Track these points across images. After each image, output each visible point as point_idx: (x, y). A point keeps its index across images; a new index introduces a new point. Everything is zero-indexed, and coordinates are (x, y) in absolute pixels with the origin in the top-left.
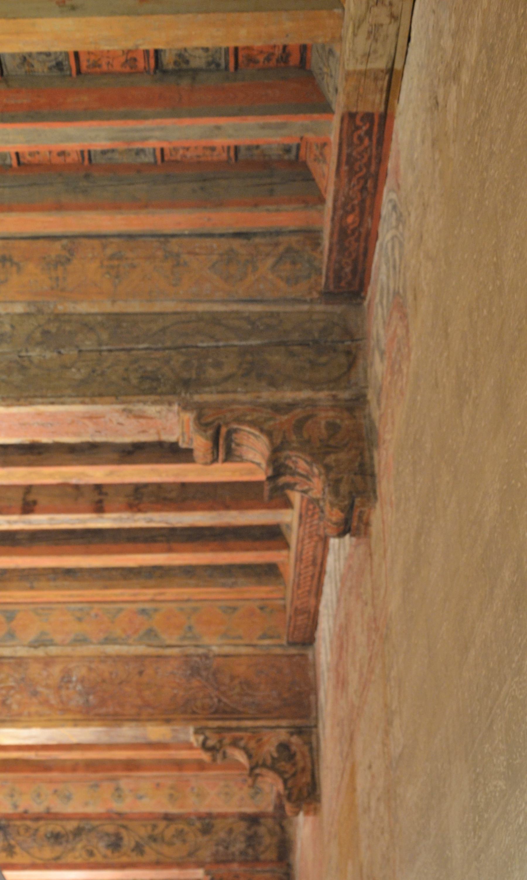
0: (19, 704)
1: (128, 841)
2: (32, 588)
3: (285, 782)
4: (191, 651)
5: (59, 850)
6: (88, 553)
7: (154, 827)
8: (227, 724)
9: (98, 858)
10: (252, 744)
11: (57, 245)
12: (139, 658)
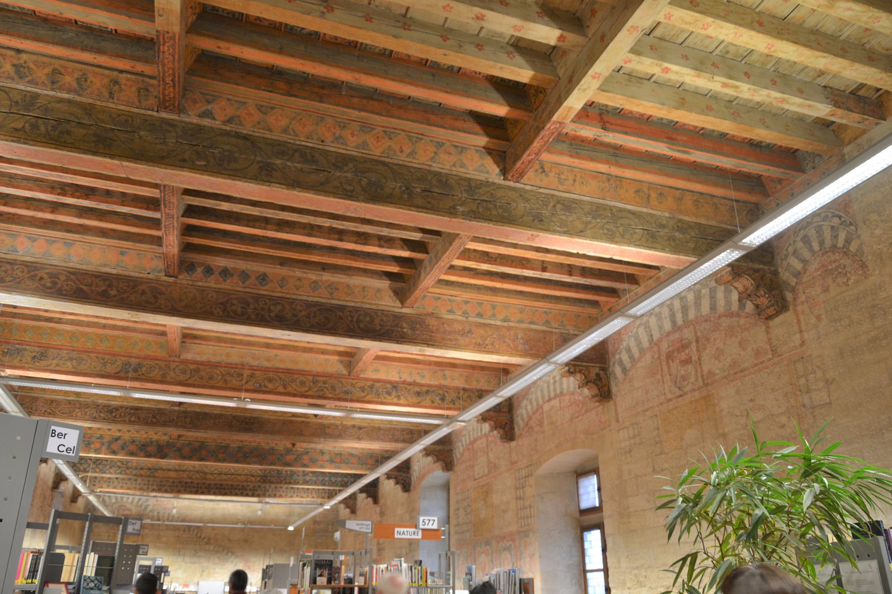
1: (448, 398)
4: (563, 331)
5: (419, 399)
6: (547, 288)
9: (436, 404)
11: (678, 192)
12: (544, 332)
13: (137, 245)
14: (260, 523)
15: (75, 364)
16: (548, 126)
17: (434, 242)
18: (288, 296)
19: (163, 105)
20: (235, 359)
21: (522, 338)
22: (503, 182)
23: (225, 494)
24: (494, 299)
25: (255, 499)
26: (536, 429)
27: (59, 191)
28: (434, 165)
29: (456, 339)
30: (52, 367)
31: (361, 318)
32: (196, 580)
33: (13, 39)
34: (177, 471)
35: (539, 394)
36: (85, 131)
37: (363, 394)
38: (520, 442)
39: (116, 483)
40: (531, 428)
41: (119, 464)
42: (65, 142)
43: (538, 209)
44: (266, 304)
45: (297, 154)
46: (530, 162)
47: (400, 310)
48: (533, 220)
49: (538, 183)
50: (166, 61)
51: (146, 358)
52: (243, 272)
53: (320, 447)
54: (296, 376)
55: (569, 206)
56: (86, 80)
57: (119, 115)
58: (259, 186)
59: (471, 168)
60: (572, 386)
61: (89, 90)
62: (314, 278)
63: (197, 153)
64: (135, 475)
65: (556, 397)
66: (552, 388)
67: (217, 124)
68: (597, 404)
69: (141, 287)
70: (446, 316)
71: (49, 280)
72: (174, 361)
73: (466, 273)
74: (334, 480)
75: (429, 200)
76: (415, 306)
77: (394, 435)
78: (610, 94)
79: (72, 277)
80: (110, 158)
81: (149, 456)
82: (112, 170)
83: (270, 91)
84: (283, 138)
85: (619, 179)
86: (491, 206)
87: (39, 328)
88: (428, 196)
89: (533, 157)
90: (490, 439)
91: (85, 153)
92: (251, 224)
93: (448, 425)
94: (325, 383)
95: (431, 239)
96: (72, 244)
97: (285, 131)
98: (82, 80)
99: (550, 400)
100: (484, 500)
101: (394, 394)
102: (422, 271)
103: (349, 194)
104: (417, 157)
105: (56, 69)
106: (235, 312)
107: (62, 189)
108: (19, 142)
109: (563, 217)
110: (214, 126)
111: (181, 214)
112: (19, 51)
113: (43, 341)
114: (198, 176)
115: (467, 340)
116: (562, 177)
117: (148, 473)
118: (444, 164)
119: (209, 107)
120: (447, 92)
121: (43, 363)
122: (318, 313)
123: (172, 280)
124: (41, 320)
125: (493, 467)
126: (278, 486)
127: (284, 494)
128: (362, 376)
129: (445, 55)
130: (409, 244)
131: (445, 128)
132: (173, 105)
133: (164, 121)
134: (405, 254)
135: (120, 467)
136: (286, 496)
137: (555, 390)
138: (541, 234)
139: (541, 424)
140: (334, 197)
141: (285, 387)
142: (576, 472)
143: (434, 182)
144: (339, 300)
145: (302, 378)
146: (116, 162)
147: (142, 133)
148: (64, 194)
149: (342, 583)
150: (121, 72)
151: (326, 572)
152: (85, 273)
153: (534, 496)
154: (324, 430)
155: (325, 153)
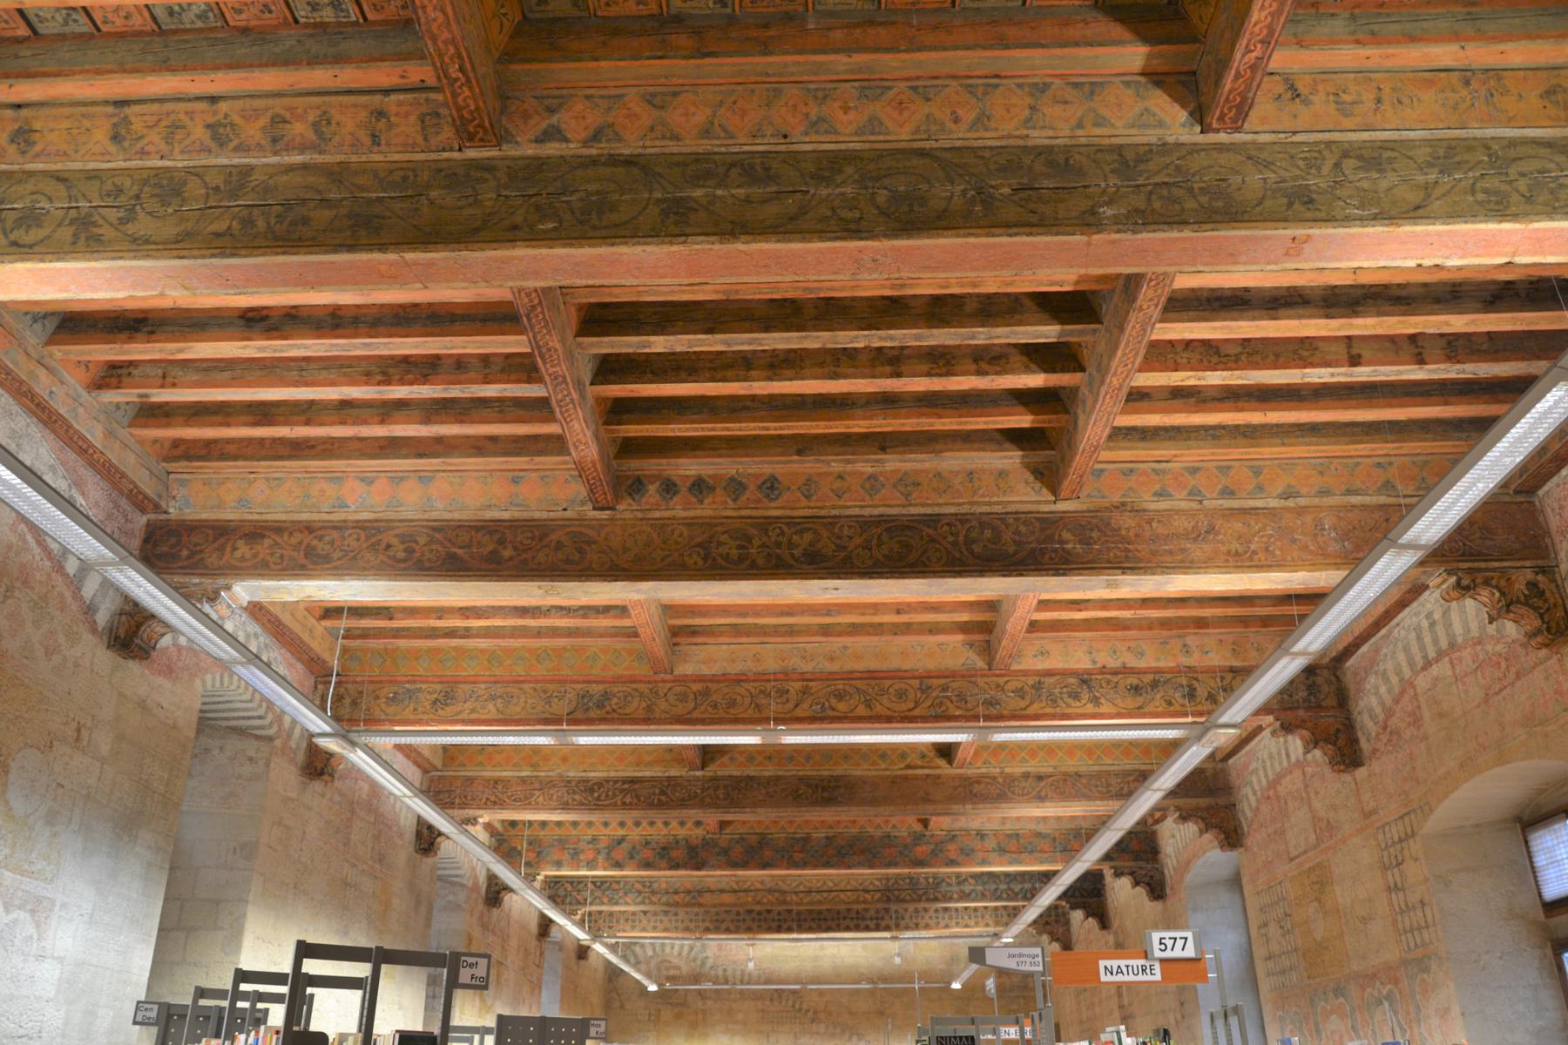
1: (1202, 692)
2: (1284, 444)
3: (1541, 616)
5: (1140, 700)
7: (1222, 678)
8: (1476, 565)
9: (1177, 707)
10: (1503, 583)
13: (537, 459)
14: (901, 979)
17: (1089, 338)
18: (823, 513)
20: (771, 665)
22: (1202, 139)
26: (1407, 734)
27: (379, 377)
28: (1035, 133)
29: (1183, 550)
30: (465, 716)
31: (973, 535)
33: (198, 76)
35: (1401, 657)
36: (334, 212)
37: (1023, 704)
38: (1376, 766)
40: (1396, 733)
41: (638, 886)
42: (300, 239)
43: (1296, 178)
44: (783, 533)
45: (734, 172)
47: (1053, 508)
48: (1290, 205)
49: (1288, 124)
51: (616, 680)
52: (732, 479)
53: (962, 823)
54: (887, 683)
55: (1374, 158)
56: (329, 123)
57: (391, 172)
58: (666, 249)
59: (1119, 124)
60: (1474, 625)
61: (337, 138)
62: (868, 469)
63: (538, 207)
64: (668, 904)
65: (1441, 654)
66: (1428, 639)
67: (573, 148)
68: (1544, 651)
69: (554, 537)
70: (1152, 506)
71: (402, 547)
72: (663, 681)
73: (1178, 402)
74: (1017, 887)
75: (1032, 206)
76: (1083, 494)
77: (1109, 785)
79: (437, 535)
80: (380, 250)
81: (676, 867)
84: (705, 146)
85: (1495, 73)
86: (1177, 192)
87: (437, 650)
88: (1028, 200)
90: (1309, 770)
92: (719, 376)
93: (1199, 738)
94: (945, 689)
95: (1082, 332)
96: (431, 479)
97: (706, 133)
99: (1428, 665)
100: (1318, 900)
101: (1085, 696)
102: (1079, 411)
103: (853, 226)
104: (993, 124)
105: (278, 115)
106: (727, 557)
107: (384, 373)
108: (222, 255)
109: (1365, 184)
110: (564, 153)
111: (587, 378)
112: (213, 99)
113: (447, 673)
114: (544, 251)
115: (1207, 547)
116: (1346, 98)
118: (1058, 126)
119: (554, 120)
122: (885, 537)
123: (606, 514)
124: (438, 637)
125: (1325, 829)
126: (920, 906)
127: (932, 923)
128: (1015, 667)
130: (1040, 356)
131: (1043, 46)
132: (481, 126)
134: (1035, 380)
135: (640, 892)
137: (1436, 642)
138: (1315, 232)
139: (1416, 721)
140: (821, 239)
142: (1518, 819)
143: (1039, 167)
144: (923, 505)
145: (900, 685)
146: (392, 256)
147: (434, 194)
150: (387, 92)
152: (460, 526)
153: (1427, 880)
155: (792, 158)
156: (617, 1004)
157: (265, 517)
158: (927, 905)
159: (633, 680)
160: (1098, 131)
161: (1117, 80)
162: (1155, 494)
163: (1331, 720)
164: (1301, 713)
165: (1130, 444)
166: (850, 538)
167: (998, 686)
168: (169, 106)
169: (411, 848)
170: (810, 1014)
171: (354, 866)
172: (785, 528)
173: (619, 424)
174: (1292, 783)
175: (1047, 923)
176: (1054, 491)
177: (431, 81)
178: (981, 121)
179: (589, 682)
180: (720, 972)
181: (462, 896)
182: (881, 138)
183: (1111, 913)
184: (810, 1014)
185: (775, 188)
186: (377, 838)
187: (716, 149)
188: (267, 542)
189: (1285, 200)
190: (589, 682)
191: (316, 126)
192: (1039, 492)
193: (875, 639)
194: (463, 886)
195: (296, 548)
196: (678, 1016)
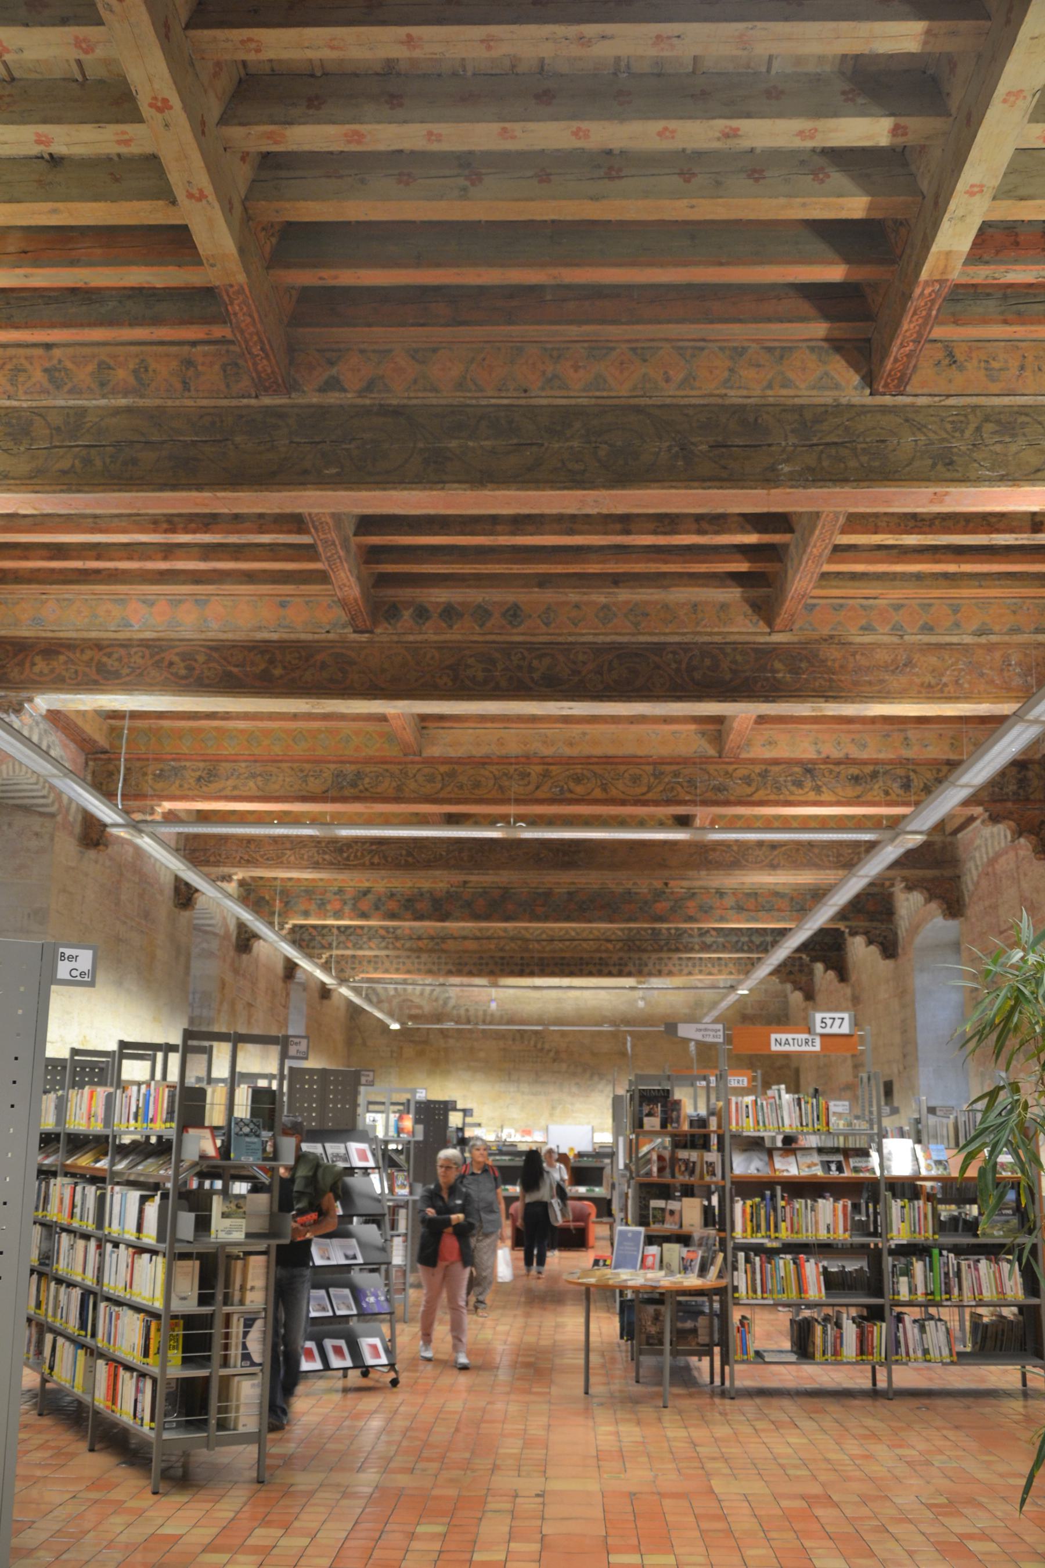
0: (970, 683)
1: (917, 783)
2: (980, 587)
5: (859, 789)
7: (939, 771)
9: (894, 797)
13: (302, 587)
15: (260, 784)
16: (917, 291)
18: (561, 639)
19: (262, 387)
20: (513, 749)
21: (1019, 664)
23: (571, 974)
24: (954, 593)
25: (630, 982)
28: (731, 393)
30: (227, 792)
32: (543, 1122)
34: (477, 938)
37: (749, 790)
39: (387, 964)
41: (382, 932)
43: (944, 440)
44: (524, 658)
46: (909, 356)
48: (934, 466)
50: (243, 325)
51: (368, 761)
52: (479, 606)
54: (623, 768)
56: (146, 370)
57: (201, 417)
58: (427, 493)
59: (803, 386)
64: (411, 950)
67: (349, 398)
70: (858, 639)
71: (182, 665)
72: (413, 763)
73: (884, 552)
76: (796, 627)
77: (839, 855)
78: (1038, 202)
79: (215, 655)
80: (197, 490)
82: (206, 505)
83: (423, 325)
87: (200, 730)
89: (911, 346)
91: (161, 490)
93: (892, 840)
94: (676, 774)
96: (206, 602)
97: (460, 386)
98: (141, 371)
101: (808, 783)
107: (169, 522)
109: (998, 448)
112: (48, 346)
113: (209, 752)
115: (904, 679)
116: (995, 365)
117: (431, 945)
118: (751, 387)
119: (334, 371)
120: (721, 264)
121: (214, 787)
123: (364, 638)
126: (664, 955)
127: (675, 969)
129: (692, 207)
131: (740, 321)
133: (268, 411)
135: (383, 938)
136: (680, 973)
140: (552, 488)
141: (604, 788)
145: (634, 770)
147: (238, 439)
148: (173, 531)
149: (686, 1127)
150: (194, 344)
151: (659, 1109)
152: (234, 646)
154: (704, 856)
156: (359, 1041)
157: (61, 635)
158: (671, 955)
159: (384, 761)
160: (784, 392)
161: (804, 345)
162: (862, 628)
163: (1037, 812)
164: (1009, 805)
165: (841, 583)
166: (584, 663)
167: (727, 773)
168: (11, 351)
169: (171, 903)
170: (552, 1054)
171: (125, 923)
172: (526, 654)
173: (378, 563)
174: (1006, 864)
175: (791, 972)
176: (770, 623)
177: (229, 336)
178: (688, 381)
179: (342, 762)
180: (462, 1012)
181: (214, 945)
182: (605, 394)
183: (850, 966)
184: (552, 1054)
185: (515, 441)
186: (141, 896)
187: (468, 402)
188: (62, 658)
189: (930, 462)
190: (342, 762)
191: (135, 372)
192: (756, 624)
193: (613, 726)
194: (215, 934)
195: (88, 663)
196: (421, 1054)
